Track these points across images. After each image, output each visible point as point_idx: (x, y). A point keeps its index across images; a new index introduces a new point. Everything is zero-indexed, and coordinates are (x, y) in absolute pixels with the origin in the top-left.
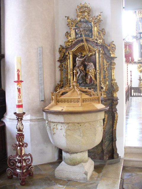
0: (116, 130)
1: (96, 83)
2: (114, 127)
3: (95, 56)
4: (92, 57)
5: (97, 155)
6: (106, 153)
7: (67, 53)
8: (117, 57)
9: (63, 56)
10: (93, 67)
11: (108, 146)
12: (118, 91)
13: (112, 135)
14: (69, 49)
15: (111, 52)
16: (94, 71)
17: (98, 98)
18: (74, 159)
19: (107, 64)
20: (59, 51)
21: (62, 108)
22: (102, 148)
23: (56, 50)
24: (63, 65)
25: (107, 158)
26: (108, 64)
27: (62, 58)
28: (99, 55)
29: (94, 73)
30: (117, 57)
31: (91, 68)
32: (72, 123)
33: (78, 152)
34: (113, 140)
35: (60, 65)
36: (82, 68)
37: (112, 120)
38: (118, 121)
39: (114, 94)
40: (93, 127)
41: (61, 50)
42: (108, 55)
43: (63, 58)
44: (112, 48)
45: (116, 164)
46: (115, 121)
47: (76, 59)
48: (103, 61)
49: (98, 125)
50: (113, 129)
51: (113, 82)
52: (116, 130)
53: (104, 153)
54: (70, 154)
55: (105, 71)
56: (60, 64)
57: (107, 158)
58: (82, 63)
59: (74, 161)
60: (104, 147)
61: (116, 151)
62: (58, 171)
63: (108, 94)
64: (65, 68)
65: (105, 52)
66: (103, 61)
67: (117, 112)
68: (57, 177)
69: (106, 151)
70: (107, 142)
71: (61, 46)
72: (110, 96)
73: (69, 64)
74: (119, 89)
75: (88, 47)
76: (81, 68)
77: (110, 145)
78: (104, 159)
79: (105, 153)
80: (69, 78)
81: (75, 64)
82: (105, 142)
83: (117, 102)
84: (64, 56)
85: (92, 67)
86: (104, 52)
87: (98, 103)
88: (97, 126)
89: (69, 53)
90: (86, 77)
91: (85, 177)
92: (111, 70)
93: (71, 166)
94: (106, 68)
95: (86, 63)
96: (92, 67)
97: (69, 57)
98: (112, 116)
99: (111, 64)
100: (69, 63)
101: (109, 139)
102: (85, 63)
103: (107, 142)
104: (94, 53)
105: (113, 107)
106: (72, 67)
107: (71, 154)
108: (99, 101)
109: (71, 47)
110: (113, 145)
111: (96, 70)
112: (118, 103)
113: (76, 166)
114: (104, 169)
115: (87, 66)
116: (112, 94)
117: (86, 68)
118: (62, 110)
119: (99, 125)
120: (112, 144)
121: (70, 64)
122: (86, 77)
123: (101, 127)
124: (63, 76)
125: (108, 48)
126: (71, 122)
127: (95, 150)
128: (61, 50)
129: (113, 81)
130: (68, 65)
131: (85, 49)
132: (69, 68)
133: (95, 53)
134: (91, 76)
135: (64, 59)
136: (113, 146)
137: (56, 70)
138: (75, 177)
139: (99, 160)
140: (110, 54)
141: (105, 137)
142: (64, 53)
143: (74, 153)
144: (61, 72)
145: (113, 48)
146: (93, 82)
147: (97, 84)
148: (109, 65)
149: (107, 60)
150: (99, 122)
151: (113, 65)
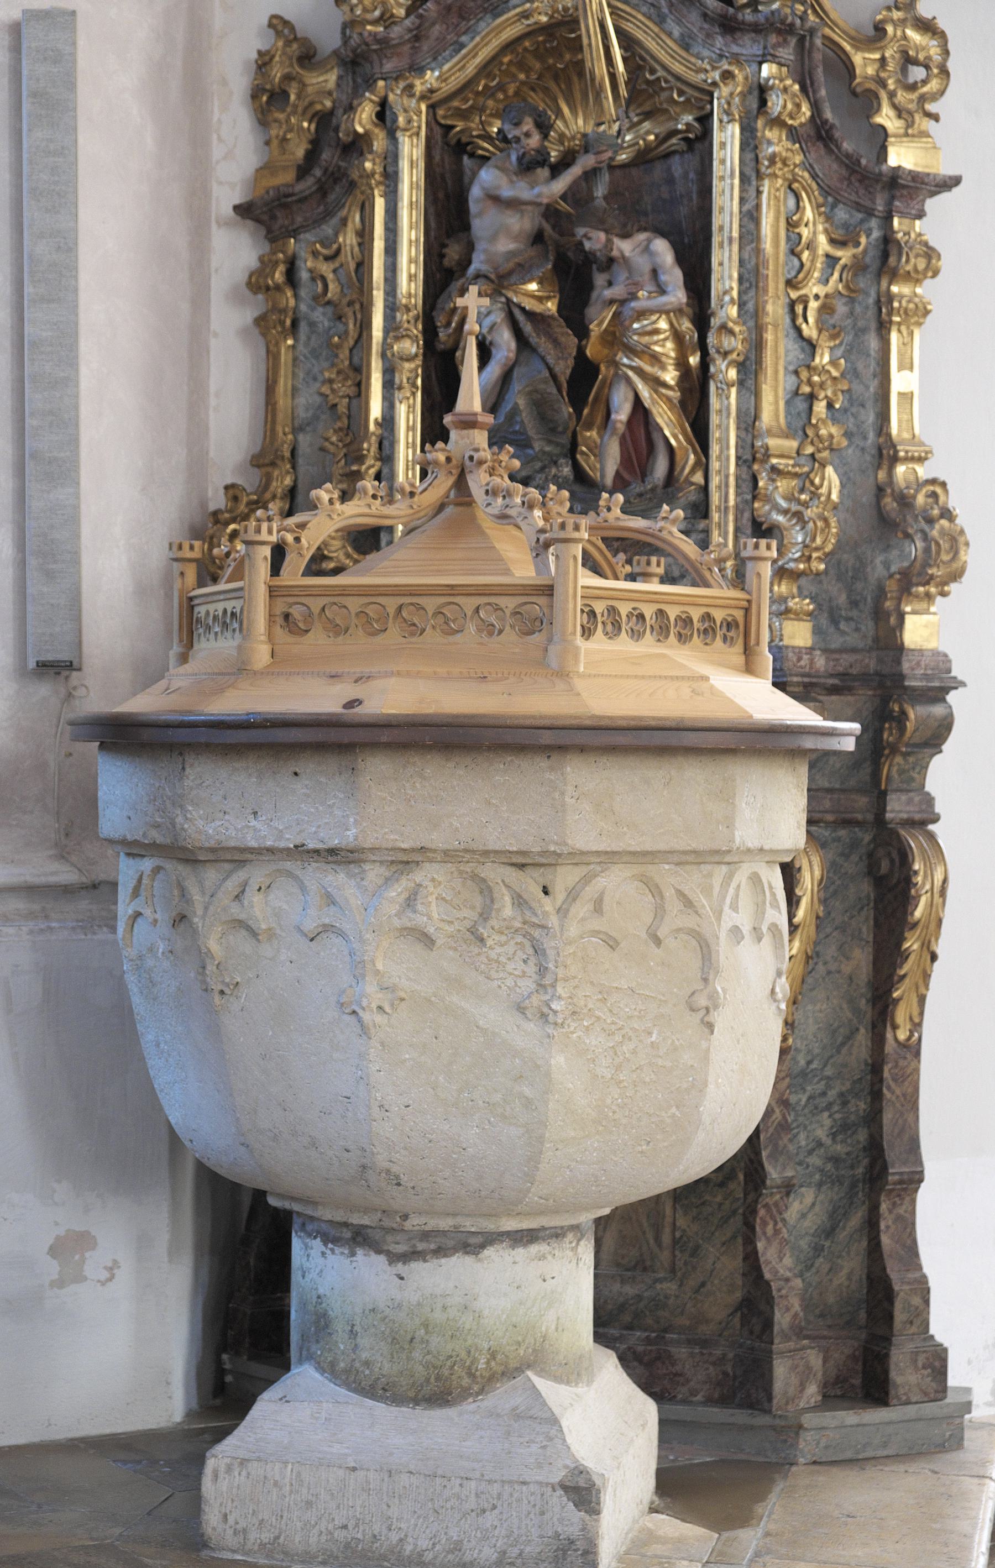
0: (917, 1054)
1: (698, 478)
2: (901, 1015)
3: (693, 160)
4: (658, 171)
5: (681, 1352)
6: (798, 1331)
7: (364, 118)
8: (955, 181)
9: (300, 153)
10: (678, 295)
11: (818, 1250)
12: (956, 576)
13: (873, 1118)
14: (388, 66)
15: (886, 118)
16: (678, 337)
17: (739, 615)
18: (438, 1316)
19: (831, 261)
20: (255, 96)
21: (347, 691)
22: (752, 1261)
23: (224, 82)
24: (307, 264)
25: (802, 1387)
26: (845, 255)
27: (288, 177)
28: (750, 143)
29: (681, 364)
30: (955, 181)
31: (644, 298)
32: (448, 856)
33: (490, 1239)
34: (885, 1168)
35: (266, 265)
36: (540, 299)
37: (877, 924)
38: (942, 947)
39: (901, 617)
40: (689, 921)
41: (288, 78)
42: (847, 146)
43: (303, 171)
44: (908, 60)
45: (922, 1466)
46: (911, 943)
47: (475, 192)
48: (791, 225)
49: (734, 907)
50: (878, 1040)
51: (901, 469)
52: (913, 1049)
53: (768, 1324)
54: (394, 1258)
55: (811, 347)
56: (266, 247)
57: (812, 1391)
58: (538, 238)
59: (435, 1341)
60: (767, 1251)
61: (921, 1315)
62: (243, 1462)
63: (834, 621)
64: (320, 299)
65: (816, 107)
66: (791, 225)
67: (932, 837)
68: (231, 1540)
69: (796, 1306)
70: (809, 1195)
71: (278, 25)
72: (852, 640)
73: (379, 245)
74: (972, 557)
75: (627, 41)
76: (531, 295)
77: (842, 1235)
78: (778, 1386)
79: (782, 1320)
80: (376, 409)
81: (453, 252)
82: (788, 1188)
83: (938, 710)
84: (312, 156)
85: (662, 291)
86: (806, 110)
87: (735, 668)
88: (730, 919)
89: (383, 114)
90: (578, 400)
91: (573, 1530)
92: (883, 328)
93: (394, 1410)
94: (826, 309)
95: (595, 240)
96: (662, 291)
97: (391, 158)
98: (880, 882)
99: (885, 255)
100: (379, 245)
101: (835, 1160)
102: (580, 231)
103: (809, 1195)
104: (689, 118)
105: (892, 768)
106: (417, 288)
107: (405, 1258)
108: (748, 651)
109: (417, 36)
110: (885, 1240)
111: (702, 319)
112: (944, 728)
113: (469, 1406)
114: (773, 1497)
115: (600, 279)
116: (879, 614)
117: (585, 302)
118: (350, 705)
119: (743, 919)
120: (872, 1224)
121: (391, 250)
122: (578, 400)
123: (767, 940)
124: (301, 401)
125: (858, 59)
126: (437, 840)
127: (670, 1287)
128: (277, 73)
129: (895, 460)
130: (364, 265)
131: (579, 68)
132: (379, 298)
133: (705, 120)
134: (645, 393)
135: (322, 191)
136: (875, 1250)
137: (215, 325)
138: (454, 1534)
139: (717, 1414)
140: (880, 138)
141: (784, 1127)
142: (324, 120)
143: (441, 1252)
144: (272, 356)
145: (917, 73)
146: (660, 468)
147: (705, 489)
148: (858, 267)
149: (841, 214)
150: (742, 876)
151: (914, 278)
